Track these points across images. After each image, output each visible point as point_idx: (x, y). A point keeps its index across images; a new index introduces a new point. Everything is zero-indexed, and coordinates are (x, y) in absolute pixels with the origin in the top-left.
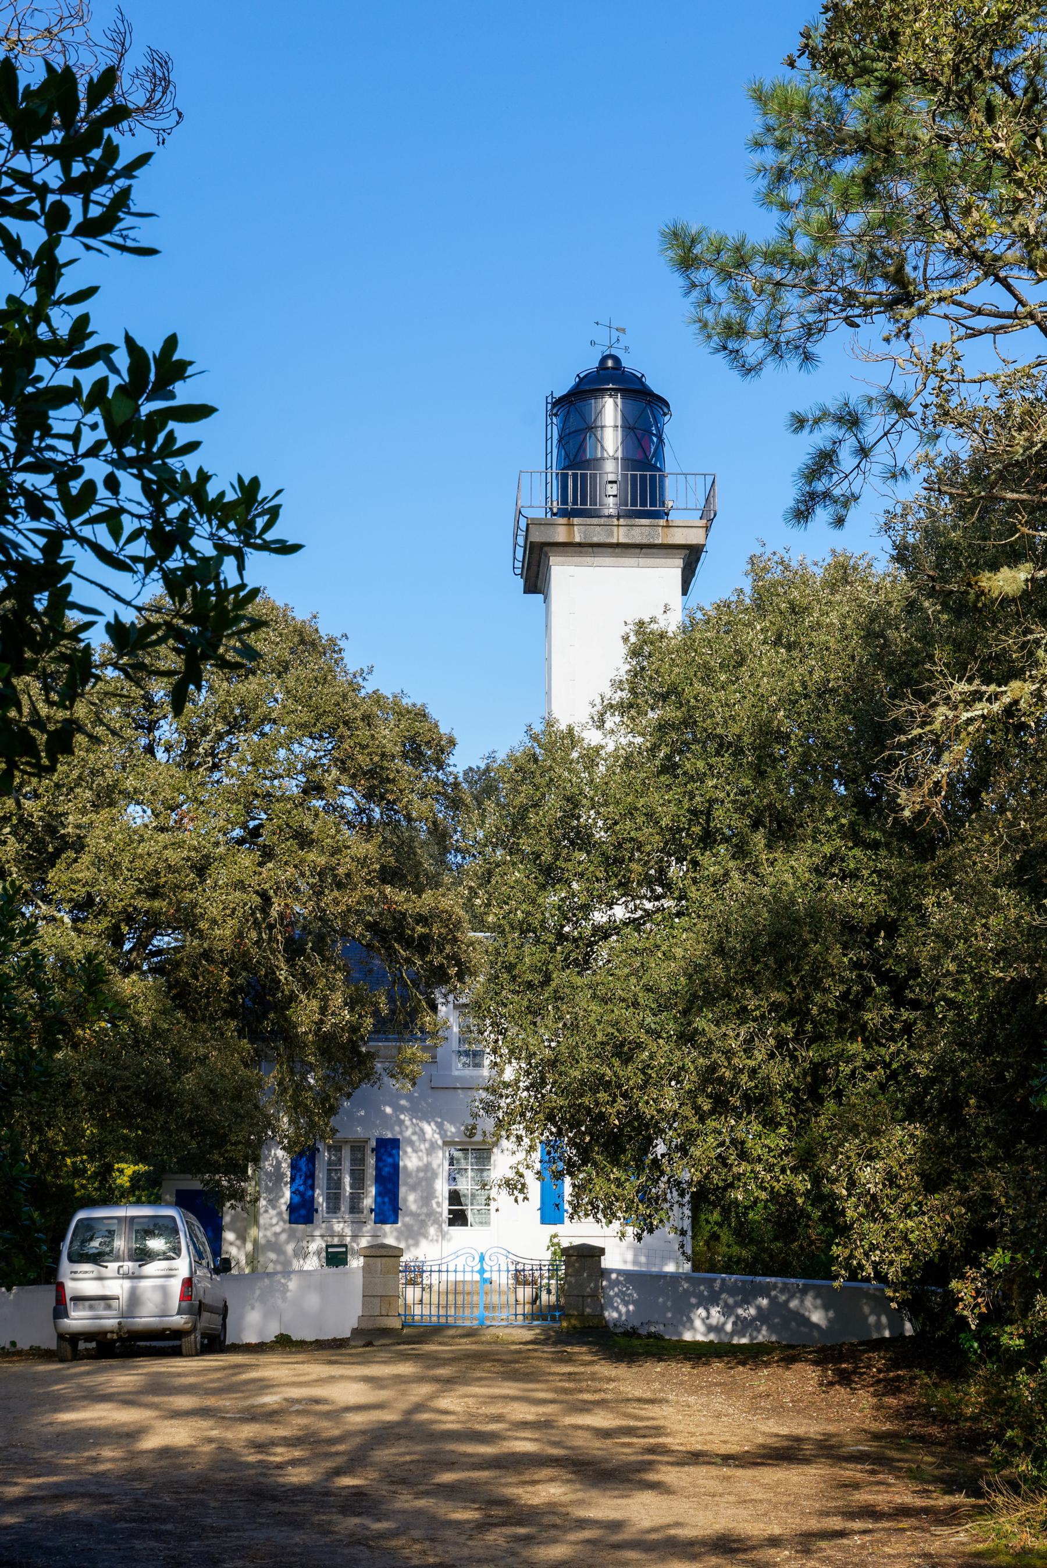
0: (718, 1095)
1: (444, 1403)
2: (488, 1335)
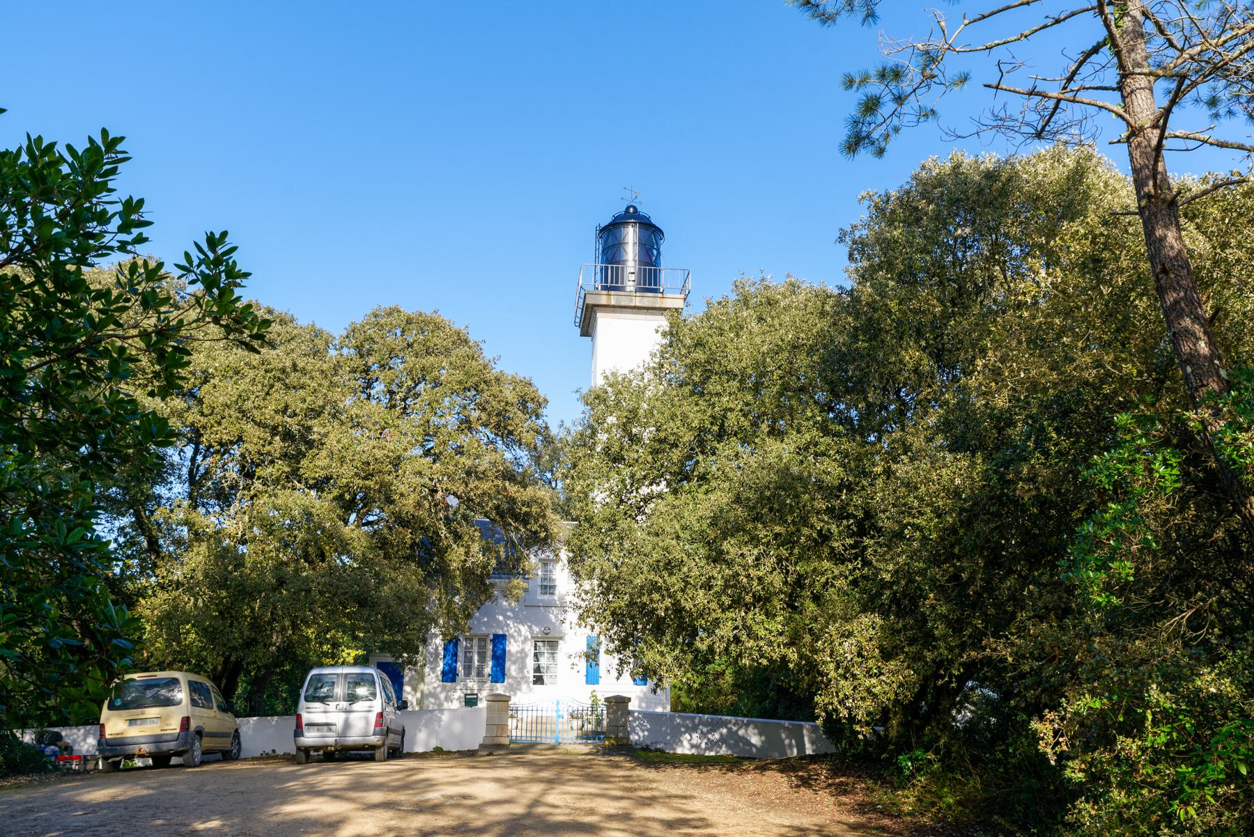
0: (738, 597)
1: (552, 798)
2: (562, 749)
